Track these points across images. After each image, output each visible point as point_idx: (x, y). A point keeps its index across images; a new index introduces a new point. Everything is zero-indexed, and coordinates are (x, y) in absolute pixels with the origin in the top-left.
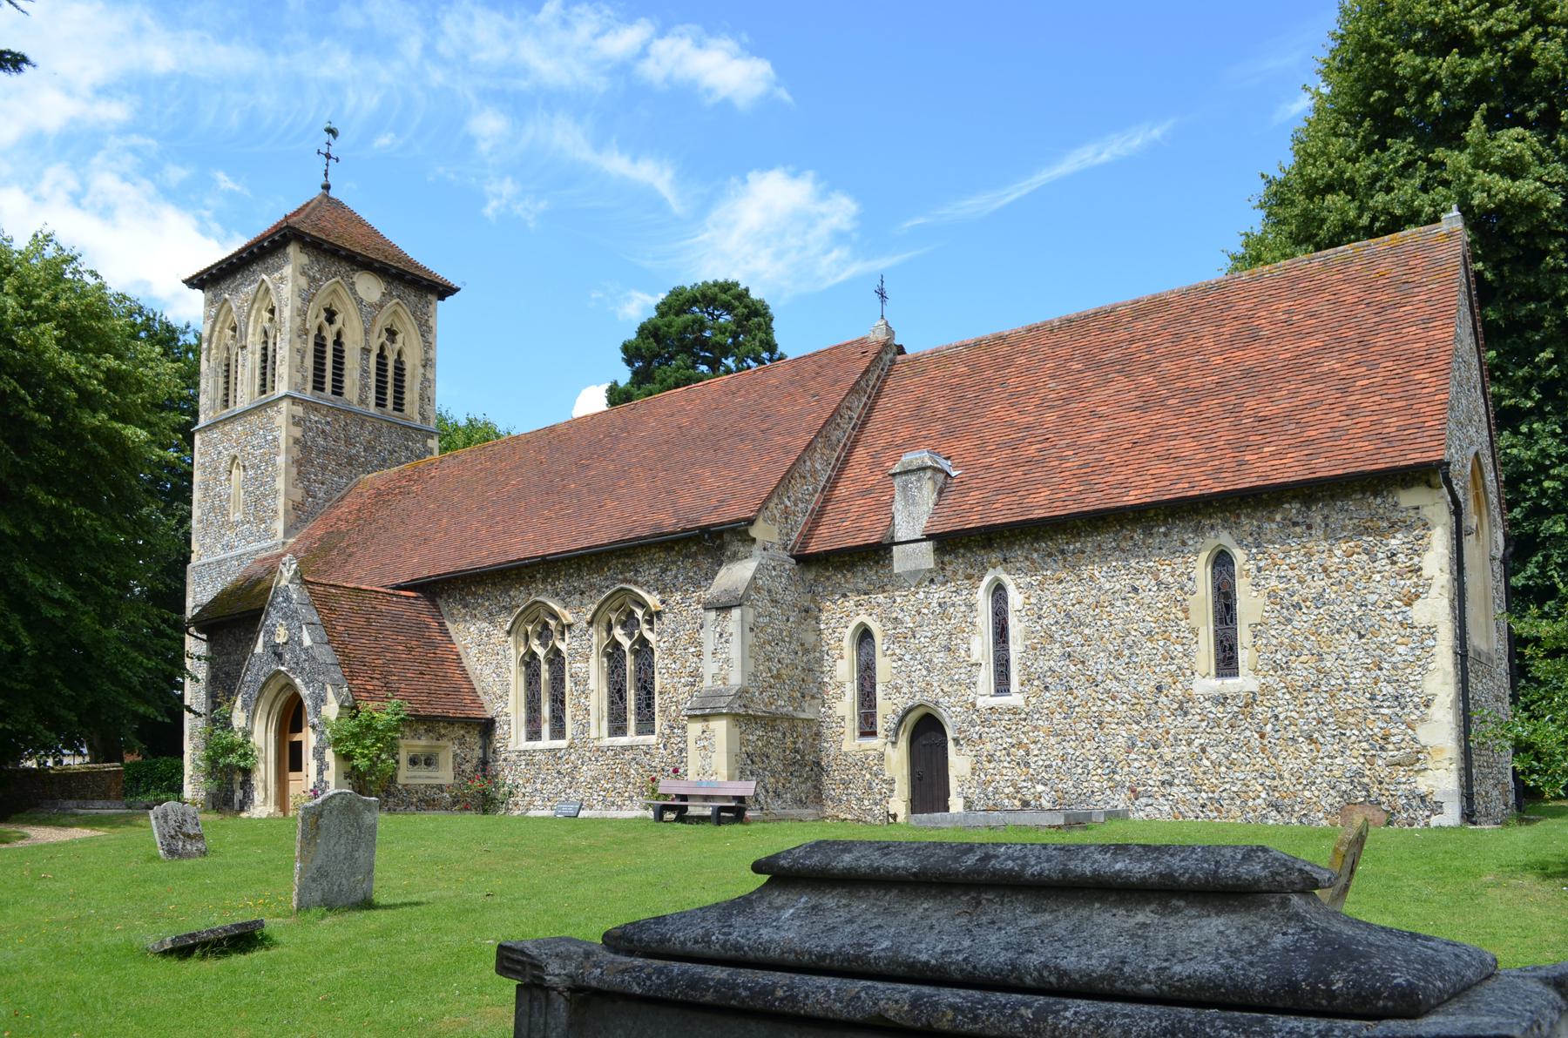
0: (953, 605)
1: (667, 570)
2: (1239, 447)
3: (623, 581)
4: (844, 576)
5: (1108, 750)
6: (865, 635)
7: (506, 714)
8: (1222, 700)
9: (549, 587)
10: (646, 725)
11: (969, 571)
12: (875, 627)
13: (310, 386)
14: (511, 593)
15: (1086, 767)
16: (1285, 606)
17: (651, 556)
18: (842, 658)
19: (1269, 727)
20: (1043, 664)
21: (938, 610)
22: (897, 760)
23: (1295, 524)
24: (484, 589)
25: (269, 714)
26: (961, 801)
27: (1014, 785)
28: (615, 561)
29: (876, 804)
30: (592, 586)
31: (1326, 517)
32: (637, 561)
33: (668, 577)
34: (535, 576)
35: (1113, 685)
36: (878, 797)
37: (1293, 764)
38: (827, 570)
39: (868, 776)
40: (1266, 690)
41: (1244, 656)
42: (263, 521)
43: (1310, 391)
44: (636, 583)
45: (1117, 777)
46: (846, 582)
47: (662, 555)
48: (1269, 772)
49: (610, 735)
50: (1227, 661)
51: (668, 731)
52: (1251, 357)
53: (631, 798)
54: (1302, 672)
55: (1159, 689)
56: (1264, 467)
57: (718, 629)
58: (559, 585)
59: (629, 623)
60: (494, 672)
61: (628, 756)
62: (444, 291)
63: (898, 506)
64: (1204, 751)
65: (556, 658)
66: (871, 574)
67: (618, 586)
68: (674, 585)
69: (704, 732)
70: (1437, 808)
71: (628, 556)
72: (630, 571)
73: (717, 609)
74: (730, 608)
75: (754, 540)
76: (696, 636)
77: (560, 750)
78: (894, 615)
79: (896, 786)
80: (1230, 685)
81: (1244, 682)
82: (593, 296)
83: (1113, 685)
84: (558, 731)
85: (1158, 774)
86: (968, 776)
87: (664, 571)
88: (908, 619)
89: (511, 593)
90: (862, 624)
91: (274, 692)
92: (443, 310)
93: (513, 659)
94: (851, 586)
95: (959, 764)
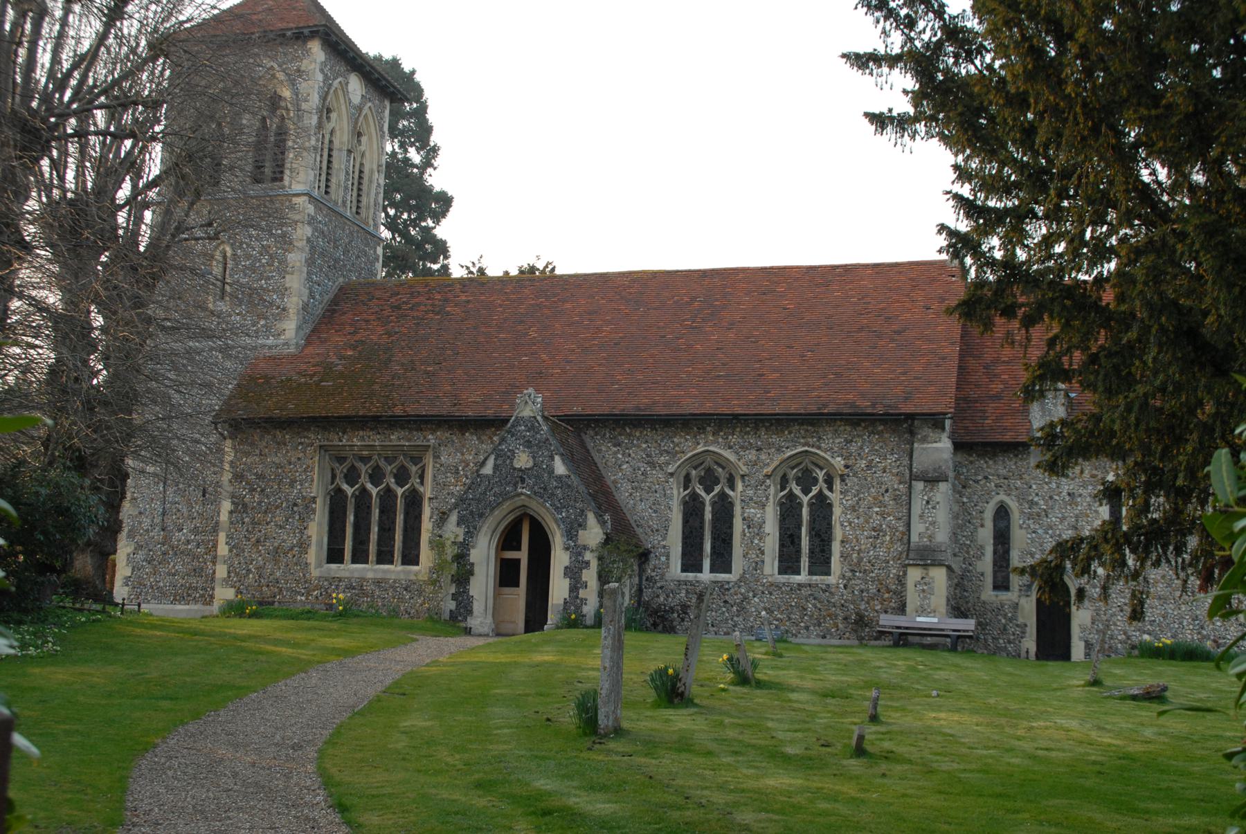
0: (1080, 495)
1: (852, 441)
3: (807, 444)
4: (986, 462)
5: (1198, 612)
6: (1002, 513)
7: (664, 547)
9: (720, 440)
10: (821, 563)
11: (1094, 472)
12: (1013, 504)
14: (675, 440)
15: (1181, 623)
17: (836, 427)
18: (982, 526)
21: (1067, 498)
24: (641, 432)
25: (494, 532)
26: (1082, 644)
27: (1125, 633)
28: (797, 427)
29: (1009, 642)
30: (770, 445)
32: (821, 429)
33: (853, 448)
34: (704, 429)
36: (1012, 637)
38: (971, 456)
39: (1003, 621)
42: (262, 316)
44: (819, 448)
45: (1204, 632)
46: (988, 467)
47: (848, 428)
49: (779, 574)
51: (849, 574)
53: (807, 628)
57: (926, 498)
58: (733, 439)
59: (807, 481)
60: (651, 508)
66: (1011, 464)
67: (800, 449)
68: (859, 454)
69: (923, 578)
71: (812, 424)
72: (813, 437)
73: (925, 481)
74: (938, 481)
76: (881, 498)
77: (728, 583)
78: (1030, 498)
79: (1028, 629)
82: (1203, 380)
84: (722, 561)
86: (1089, 624)
87: (848, 442)
88: (1042, 502)
89: (675, 440)
90: (1002, 502)
91: (505, 513)
93: (675, 497)
94: (993, 471)
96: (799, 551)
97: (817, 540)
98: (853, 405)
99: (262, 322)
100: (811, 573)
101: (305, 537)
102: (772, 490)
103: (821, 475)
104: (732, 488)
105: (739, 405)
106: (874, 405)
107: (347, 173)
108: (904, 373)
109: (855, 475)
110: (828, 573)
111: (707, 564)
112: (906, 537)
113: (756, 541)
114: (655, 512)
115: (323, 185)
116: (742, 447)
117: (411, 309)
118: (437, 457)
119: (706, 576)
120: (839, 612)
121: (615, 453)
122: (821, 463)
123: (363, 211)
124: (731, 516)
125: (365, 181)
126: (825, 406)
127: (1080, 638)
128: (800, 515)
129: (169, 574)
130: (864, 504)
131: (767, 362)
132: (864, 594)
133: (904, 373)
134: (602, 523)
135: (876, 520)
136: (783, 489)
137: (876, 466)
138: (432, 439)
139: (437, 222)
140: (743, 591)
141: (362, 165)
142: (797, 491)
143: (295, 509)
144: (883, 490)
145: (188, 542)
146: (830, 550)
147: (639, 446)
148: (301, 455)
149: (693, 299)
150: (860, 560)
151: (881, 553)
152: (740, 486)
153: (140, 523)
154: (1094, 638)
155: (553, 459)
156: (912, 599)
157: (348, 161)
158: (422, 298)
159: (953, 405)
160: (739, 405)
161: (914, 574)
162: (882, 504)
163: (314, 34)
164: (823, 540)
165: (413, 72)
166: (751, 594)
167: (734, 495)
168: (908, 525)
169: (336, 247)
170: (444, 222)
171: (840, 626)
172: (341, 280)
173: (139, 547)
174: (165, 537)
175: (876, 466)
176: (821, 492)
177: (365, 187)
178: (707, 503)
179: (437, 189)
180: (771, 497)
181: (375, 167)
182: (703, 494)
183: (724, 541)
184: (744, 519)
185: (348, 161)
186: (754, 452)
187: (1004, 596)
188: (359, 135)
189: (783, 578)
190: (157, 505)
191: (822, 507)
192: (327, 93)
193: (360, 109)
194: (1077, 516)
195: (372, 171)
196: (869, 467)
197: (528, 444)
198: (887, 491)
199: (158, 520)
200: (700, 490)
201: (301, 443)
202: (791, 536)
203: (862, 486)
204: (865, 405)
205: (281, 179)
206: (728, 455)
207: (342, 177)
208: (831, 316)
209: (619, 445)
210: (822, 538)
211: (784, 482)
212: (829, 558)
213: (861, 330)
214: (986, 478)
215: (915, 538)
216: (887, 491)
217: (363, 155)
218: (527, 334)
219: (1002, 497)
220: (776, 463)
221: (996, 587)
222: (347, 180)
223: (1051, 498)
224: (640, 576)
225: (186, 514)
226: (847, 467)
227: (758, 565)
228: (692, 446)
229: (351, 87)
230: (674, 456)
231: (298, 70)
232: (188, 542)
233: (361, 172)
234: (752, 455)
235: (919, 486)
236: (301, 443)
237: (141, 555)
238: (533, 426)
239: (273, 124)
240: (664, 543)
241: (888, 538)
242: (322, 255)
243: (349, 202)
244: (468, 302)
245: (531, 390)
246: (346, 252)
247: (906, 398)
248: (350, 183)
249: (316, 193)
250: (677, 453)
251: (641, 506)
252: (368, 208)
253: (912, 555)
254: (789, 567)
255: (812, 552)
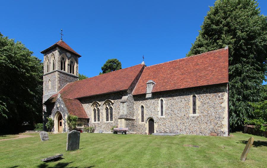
2: (197, 80)
8: (194, 117)
13: (60, 69)
16: (203, 104)
19: (200, 121)
20: (168, 112)
22: (147, 125)
23: (205, 92)
31: (209, 91)
35: (178, 115)
37: (204, 127)
40: (200, 116)
41: (197, 111)
43: (207, 72)
48: (200, 128)
50: (194, 112)
52: (197, 67)
54: (205, 113)
55: (184, 115)
56: (201, 83)
61: (109, 124)
62: (79, 56)
63: (147, 88)
64: (191, 124)
65: (98, 110)
70: (225, 133)
75: (127, 93)
80: (195, 115)
81: (197, 115)
83: (178, 115)
84: (99, 120)
85: (184, 128)
92: (79, 59)
95: (156, 126)
249: (60, 70)
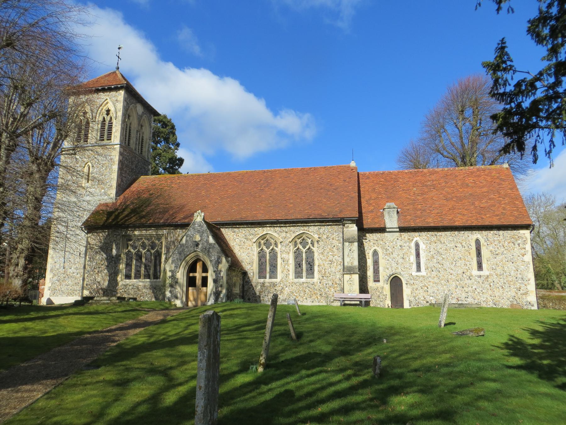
27: (424, 297)
29: (381, 301)
33: (321, 231)
39: (378, 294)
44: (309, 231)
49: (295, 278)
51: (321, 278)
53: (306, 299)
79: (388, 296)
84: (273, 274)
96: (302, 270)
97: (309, 266)
98: (321, 215)
99: (103, 191)
100: (307, 278)
101: (116, 270)
102: (292, 247)
103: (309, 241)
104: (277, 247)
105: (279, 216)
106: (328, 215)
107: (137, 139)
108: (339, 203)
109: (322, 241)
110: (313, 278)
111: (268, 275)
112: (342, 264)
113: (286, 267)
114: (249, 257)
115: (127, 142)
116: (280, 232)
117: (159, 186)
118: (166, 238)
119: (268, 280)
120: (318, 292)
121: (233, 235)
122: (310, 237)
123: (143, 153)
124: (277, 258)
125: (144, 143)
126: (310, 215)
127: (407, 300)
128: (302, 256)
129: (66, 285)
130: (326, 252)
131: (288, 201)
132: (327, 285)
133: (339, 203)
134: (228, 261)
135: (331, 257)
136: (295, 246)
137: (330, 237)
138: (165, 232)
139: (179, 167)
140: (282, 285)
141: (143, 137)
142: (301, 247)
143: (113, 259)
144: (333, 246)
145: (74, 273)
146: (314, 269)
147: (242, 232)
148: (115, 239)
149: (261, 180)
150: (325, 272)
151: (333, 269)
152: (279, 246)
153: (55, 266)
154: (412, 299)
155: (208, 237)
156: (346, 288)
157: (137, 134)
158: (163, 182)
159: (358, 214)
160: (279, 216)
161: (347, 277)
162: (333, 251)
163: (121, 88)
164: (311, 265)
165: (171, 120)
166: (285, 287)
167: (278, 250)
168: (343, 259)
169: (132, 164)
170: (182, 167)
171: (319, 298)
172: (134, 176)
173: (54, 275)
174: (65, 271)
175: (330, 237)
176: (309, 248)
177: (144, 145)
178: (268, 253)
179: (178, 157)
180: (291, 250)
181: (148, 138)
182: (266, 249)
183: (274, 267)
184: (282, 258)
185: (137, 134)
186: (284, 233)
187: (378, 284)
188: (142, 126)
189: (297, 280)
190: (62, 259)
191: (310, 252)
192: (128, 109)
193: (141, 116)
194: (403, 254)
195: (147, 139)
196: (327, 238)
197: (199, 231)
198: (334, 246)
199: (62, 265)
200: (265, 248)
201: (115, 234)
202: (299, 264)
203: (325, 245)
204: (325, 215)
205: (110, 139)
206: (275, 234)
207: (135, 139)
208: (310, 184)
209: (235, 232)
210: (274, 267)
211: (296, 245)
212: (313, 272)
213: (322, 189)
214: (370, 241)
215: (346, 264)
216: (334, 246)
217: (143, 133)
218: (201, 193)
219: (376, 248)
220: (293, 237)
221: (375, 281)
222: (136, 141)
223: (394, 247)
224: (243, 281)
225: (73, 262)
226: (319, 238)
227: (287, 276)
228: (261, 231)
229: (138, 109)
230: (255, 236)
231: (117, 100)
232: (74, 273)
233: (142, 139)
234: (284, 234)
235: (347, 244)
236: (115, 234)
237: (55, 278)
238: (200, 225)
239: (108, 119)
240: (252, 268)
241: (335, 264)
242: (127, 166)
243: (137, 149)
244: (180, 183)
245: (200, 211)
246: (136, 167)
247: (340, 212)
248: (138, 142)
250: (256, 234)
251: (243, 255)
252: (145, 152)
253: (345, 270)
254: (299, 276)
255: (307, 270)
